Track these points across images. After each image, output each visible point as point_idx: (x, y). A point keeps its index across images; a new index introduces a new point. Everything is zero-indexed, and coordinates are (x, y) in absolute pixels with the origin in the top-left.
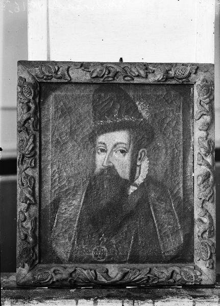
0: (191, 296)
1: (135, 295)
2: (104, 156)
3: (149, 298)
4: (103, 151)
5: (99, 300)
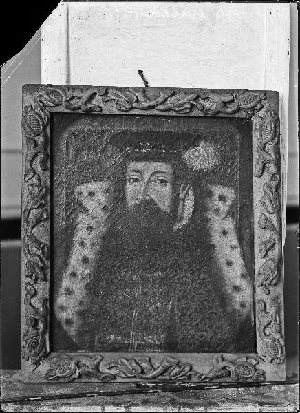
1: (182, 400)
4: (136, 180)
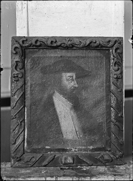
5: (58, 178)
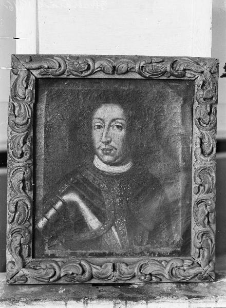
0: (187, 296)
2: (101, 132)
3: (142, 299)
4: (99, 127)
5: (89, 301)
